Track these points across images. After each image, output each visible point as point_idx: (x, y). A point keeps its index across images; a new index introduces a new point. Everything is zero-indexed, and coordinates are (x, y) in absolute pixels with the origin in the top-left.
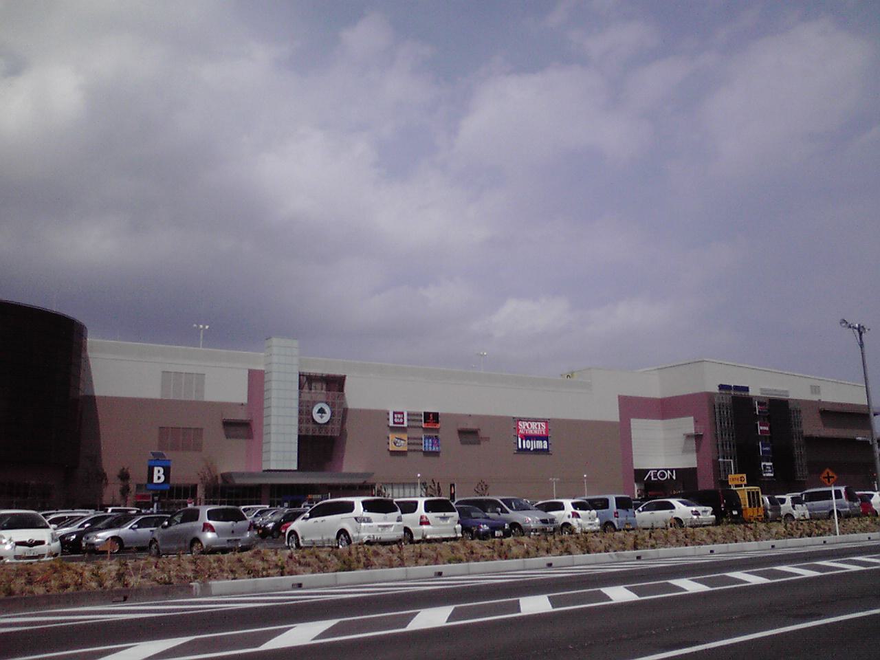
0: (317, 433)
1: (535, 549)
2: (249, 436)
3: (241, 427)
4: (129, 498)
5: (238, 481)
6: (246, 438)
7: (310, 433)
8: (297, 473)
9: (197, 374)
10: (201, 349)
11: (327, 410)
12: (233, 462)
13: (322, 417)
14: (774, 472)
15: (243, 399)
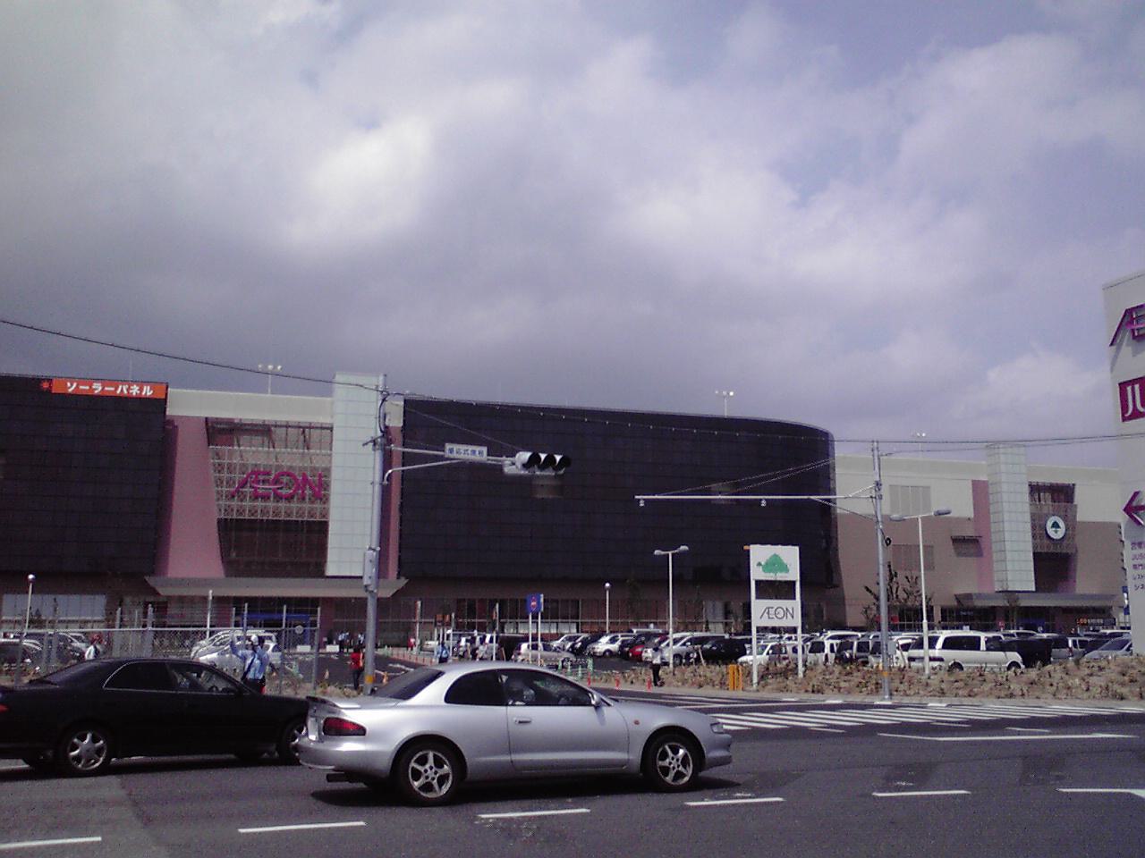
0: (1052, 550)
1: (985, 684)
2: (979, 554)
3: (970, 544)
4: (302, 695)
5: (979, 603)
6: (977, 556)
7: (1045, 550)
8: (1037, 594)
9: (902, 487)
10: (117, 629)
11: (1062, 524)
12: (964, 582)
13: (1056, 532)
14: (744, 647)
15: (970, 513)
